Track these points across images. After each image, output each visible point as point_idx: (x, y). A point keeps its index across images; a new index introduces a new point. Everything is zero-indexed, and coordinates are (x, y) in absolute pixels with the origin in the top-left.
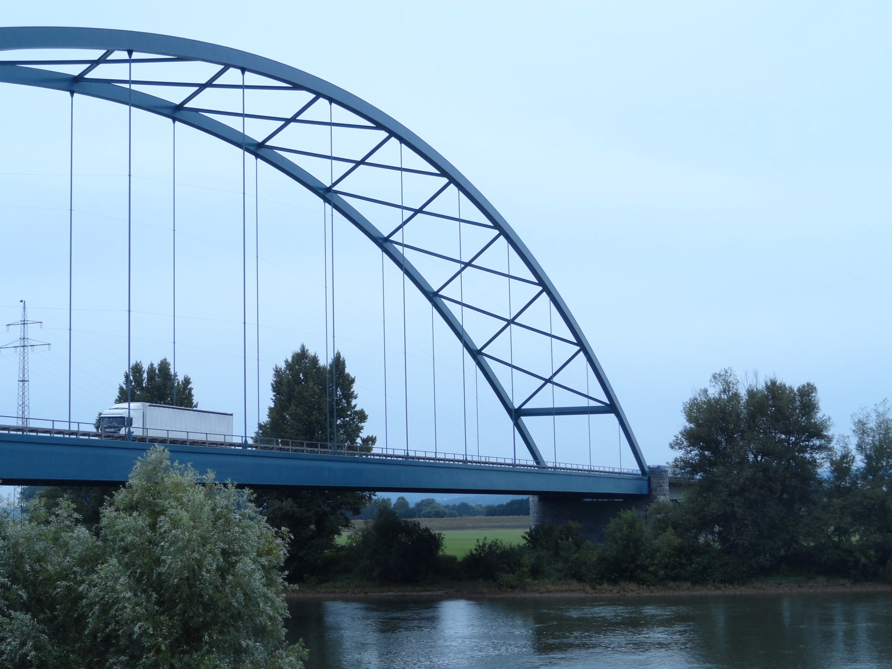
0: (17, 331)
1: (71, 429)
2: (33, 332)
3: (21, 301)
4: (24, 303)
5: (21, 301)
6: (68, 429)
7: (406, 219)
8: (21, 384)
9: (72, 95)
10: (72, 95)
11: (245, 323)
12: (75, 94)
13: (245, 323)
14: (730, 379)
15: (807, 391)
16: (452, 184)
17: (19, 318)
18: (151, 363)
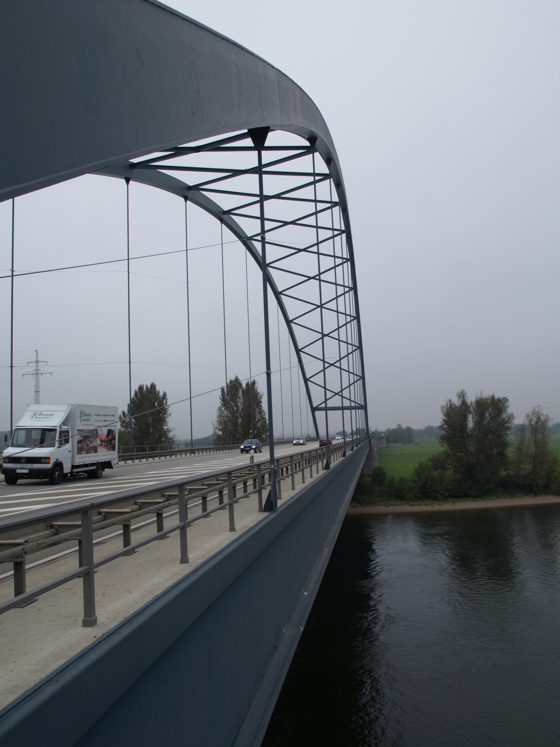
0: (33, 366)
1: (344, 406)
2: (42, 368)
3: (36, 351)
4: (37, 352)
5: (36, 351)
6: (349, 405)
7: (282, 298)
8: (36, 393)
9: (128, 183)
10: (128, 183)
11: (130, 363)
12: (131, 182)
13: (130, 363)
14: (458, 397)
15: (153, 386)
16: (260, 220)
17: (34, 359)
18: (146, 385)
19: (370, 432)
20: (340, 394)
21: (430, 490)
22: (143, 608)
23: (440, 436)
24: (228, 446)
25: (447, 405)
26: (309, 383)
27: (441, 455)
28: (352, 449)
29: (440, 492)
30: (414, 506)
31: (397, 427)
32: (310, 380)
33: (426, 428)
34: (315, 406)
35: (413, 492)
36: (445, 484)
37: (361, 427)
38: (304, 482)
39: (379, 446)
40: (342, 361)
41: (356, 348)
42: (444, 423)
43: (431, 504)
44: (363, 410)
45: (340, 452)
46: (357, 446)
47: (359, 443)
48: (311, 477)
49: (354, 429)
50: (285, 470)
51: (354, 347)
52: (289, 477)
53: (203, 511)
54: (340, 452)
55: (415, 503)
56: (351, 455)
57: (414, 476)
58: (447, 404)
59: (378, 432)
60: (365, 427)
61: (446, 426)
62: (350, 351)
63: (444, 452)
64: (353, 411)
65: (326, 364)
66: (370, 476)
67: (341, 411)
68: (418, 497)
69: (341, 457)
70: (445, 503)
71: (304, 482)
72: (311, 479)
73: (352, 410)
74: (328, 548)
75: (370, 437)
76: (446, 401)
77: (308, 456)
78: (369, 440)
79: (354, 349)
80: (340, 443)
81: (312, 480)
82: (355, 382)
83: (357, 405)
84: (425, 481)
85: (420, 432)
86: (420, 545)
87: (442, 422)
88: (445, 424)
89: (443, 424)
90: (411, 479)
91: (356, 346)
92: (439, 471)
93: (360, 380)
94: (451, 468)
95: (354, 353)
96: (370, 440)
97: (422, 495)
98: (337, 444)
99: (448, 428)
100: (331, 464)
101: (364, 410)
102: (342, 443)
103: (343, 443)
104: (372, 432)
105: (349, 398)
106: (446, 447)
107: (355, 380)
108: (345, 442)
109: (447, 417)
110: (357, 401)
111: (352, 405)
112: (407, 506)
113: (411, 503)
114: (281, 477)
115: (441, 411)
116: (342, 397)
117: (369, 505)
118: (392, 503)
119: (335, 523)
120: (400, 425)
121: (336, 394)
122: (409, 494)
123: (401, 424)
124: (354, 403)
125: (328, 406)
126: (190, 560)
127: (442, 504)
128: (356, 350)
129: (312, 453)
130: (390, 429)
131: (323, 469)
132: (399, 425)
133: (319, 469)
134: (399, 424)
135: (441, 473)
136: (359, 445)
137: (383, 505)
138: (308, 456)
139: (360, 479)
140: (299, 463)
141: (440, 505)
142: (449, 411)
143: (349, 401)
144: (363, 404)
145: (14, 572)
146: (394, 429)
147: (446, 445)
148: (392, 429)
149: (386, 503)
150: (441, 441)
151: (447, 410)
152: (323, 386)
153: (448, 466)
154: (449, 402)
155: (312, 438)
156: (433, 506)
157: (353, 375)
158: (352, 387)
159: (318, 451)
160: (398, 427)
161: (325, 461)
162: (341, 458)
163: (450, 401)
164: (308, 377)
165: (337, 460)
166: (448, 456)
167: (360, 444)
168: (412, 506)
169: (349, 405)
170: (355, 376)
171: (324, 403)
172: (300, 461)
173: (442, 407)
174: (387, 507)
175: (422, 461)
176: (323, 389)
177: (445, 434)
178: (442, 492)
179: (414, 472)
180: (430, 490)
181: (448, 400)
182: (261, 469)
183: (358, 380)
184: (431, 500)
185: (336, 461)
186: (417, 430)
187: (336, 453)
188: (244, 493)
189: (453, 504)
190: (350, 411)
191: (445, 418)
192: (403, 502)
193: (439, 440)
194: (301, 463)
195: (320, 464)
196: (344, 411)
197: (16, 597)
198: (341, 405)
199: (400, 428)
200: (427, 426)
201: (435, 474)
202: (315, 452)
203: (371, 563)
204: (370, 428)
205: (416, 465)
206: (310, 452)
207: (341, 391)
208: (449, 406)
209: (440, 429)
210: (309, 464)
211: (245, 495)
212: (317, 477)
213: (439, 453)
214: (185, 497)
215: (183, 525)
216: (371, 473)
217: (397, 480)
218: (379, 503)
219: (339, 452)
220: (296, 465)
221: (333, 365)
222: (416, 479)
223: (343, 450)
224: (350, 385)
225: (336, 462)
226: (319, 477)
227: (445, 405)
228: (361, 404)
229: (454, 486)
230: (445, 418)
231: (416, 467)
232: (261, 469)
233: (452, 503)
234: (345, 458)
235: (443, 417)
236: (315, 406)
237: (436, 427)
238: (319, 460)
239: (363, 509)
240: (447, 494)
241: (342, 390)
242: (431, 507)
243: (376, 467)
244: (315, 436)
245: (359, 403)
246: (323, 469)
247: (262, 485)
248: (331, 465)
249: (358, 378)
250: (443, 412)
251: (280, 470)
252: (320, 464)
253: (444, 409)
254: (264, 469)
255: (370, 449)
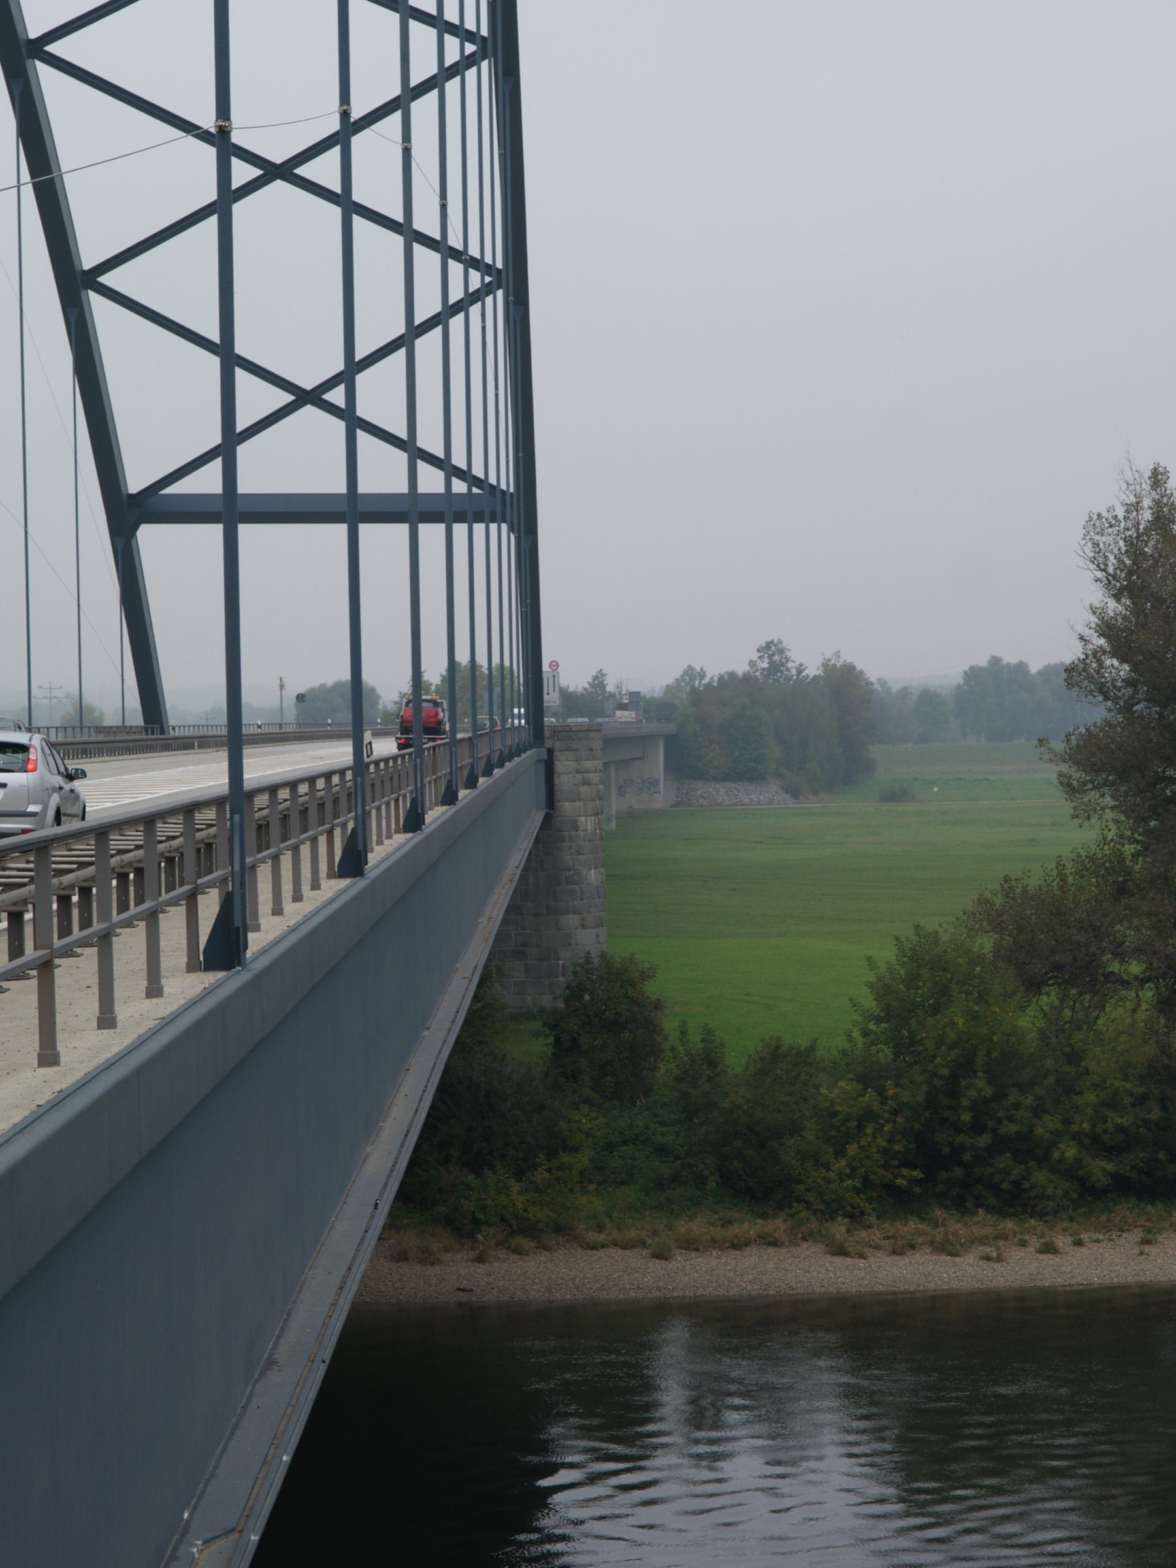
1: (363, 488)
6: (404, 488)
19: (551, 698)
20: (336, 396)
21: (985, 1140)
22: (178, 1013)
23: (1074, 742)
24: (150, 737)
25: (1136, 506)
26: (98, 305)
27: (1070, 879)
28: (414, 822)
29: (1056, 1155)
30: (862, 1256)
31: (752, 664)
32: (105, 279)
33: (973, 674)
34: (136, 481)
35: (852, 1149)
36: (1092, 1097)
37: (482, 659)
38: (48, 1056)
39: (616, 804)
40: (358, 142)
41: (470, 48)
42: (1102, 641)
43: (982, 1241)
44: (504, 526)
45: (322, 841)
46: (449, 798)
47: (466, 772)
48: (107, 1020)
49: (434, 670)
50: (29, 920)
51: (451, 42)
52: (27, 977)
53: (80, 927)
54: (322, 841)
55: (864, 1234)
56: (404, 864)
57: (866, 1033)
58: (1133, 499)
59: (612, 695)
60: (512, 658)
61: (1117, 669)
62: (423, 68)
63: (1092, 858)
64: (432, 534)
65: (237, 181)
66: (537, 1025)
67: (340, 531)
68: (890, 1187)
69: (330, 876)
70: (1084, 1236)
71: (48, 1056)
72: (277, 918)
73: (424, 529)
74: (215, 1546)
75: (547, 733)
76: (1129, 477)
77: (83, 865)
78: (544, 755)
79: (452, 55)
80: (328, 776)
81: (112, 1043)
82: (451, 310)
83: (459, 487)
84: (945, 1072)
85: (928, 699)
86: (881, 1501)
87: (1087, 633)
88: (1114, 655)
89: (1097, 654)
90: (844, 1052)
91: (470, 36)
92: (1048, 999)
93: (489, 300)
94: (1143, 982)
95: (452, 87)
96: (550, 752)
97: (917, 1174)
98: (302, 780)
99: (1128, 683)
100: (257, 928)
101: (511, 529)
102: (342, 772)
103: (349, 775)
104: (566, 695)
105: (403, 434)
106: (1111, 825)
107: (456, 294)
108: (360, 764)
109: (1132, 597)
110: (459, 460)
111: (422, 488)
112: (806, 1249)
113: (839, 1228)
114: (57, 943)
115: (1089, 550)
116: (354, 423)
117: (522, 1241)
118: (696, 1226)
119: (271, 1363)
120: (781, 651)
121: (304, 397)
122: (827, 1167)
123: (786, 643)
124: (439, 475)
125: (244, 486)
126: (262, 926)
127: (1062, 1241)
128: (469, 61)
129: (116, 842)
130: (702, 675)
131: (192, 967)
132: (771, 649)
133: (165, 962)
134: (769, 645)
135: (1067, 1013)
136: (463, 793)
137: (626, 1246)
138: (83, 865)
139: (461, 1047)
140: (85, 892)
141: (1049, 1249)
142: (1144, 554)
143: (402, 457)
144: (504, 479)
145: (9, 925)
146: (732, 675)
147: (1113, 808)
148: (721, 678)
149: (655, 1233)
150: (1078, 775)
151: (1134, 548)
152: (215, 336)
153: (1122, 961)
154: (1146, 486)
155: (109, 730)
156: (1000, 1259)
157: (435, 257)
158: (428, 346)
159: (163, 829)
160: (765, 664)
161: (209, 907)
162: (332, 887)
163: (1158, 478)
164: (89, 259)
165: (297, 897)
166: (1122, 891)
167: (471, 783)
168: (842, 1252)
169: (404, 488)
170: (455, 268)
171: (217, 464)
172: (25, 902)
173: (1097, 524)
174: (661, 1255)
175: (931, 925)
176: (212, 363)
177: (1108, 724)
178: (1070, 1151)
179: (869, 1002)
180: (985, 1140)
181: (1148, 474)
182: (197, 826)
183: (473, 298)
184: (990, 1210)
185: (289, 907)
186: (905, 692)
187: (296, 849)
188: (11, 959)
189: (1147, 1242)
190: (403, 529)
191: (1113, 607)
192: (778, 1225)
193: (1064, 768)
194: (28, 916)
195: (173, 924)
196: (364, 529)
197: (138, 908)
198: (339, 486)
199: (775, 668)
200: (983, 662)
201: (1024, 1022)
202: (136, 836)
203: (545, 1483)
204: (555, 665)
205: (887, 954)
206: (148, 821)
207: (347, 376)
208: (1147, 515)
209: (1070, 683)
210: (140, 901)
211: (170, 899)
212: (151, 1024)
213: (1060, 866)
214: (109, 861)
215: (105, 928)
216: (546, 1001)
217: (736, 1062)
218: (600, 1228)
219: (314, 840)
220: (64, 901)
221: (285, 171)
222: (885, 1053)
223: (344, 825)
224: (415, 331)
225: (294, 912)
226: (167, 1022)
227: (1120, 512)
228: (492, 480)
229: (1155, 1114)
230: (1113, 607)
231: (883, 968)
232: (197, 826)
233: (1137, 1235)
234: (362, 883)
235: (1097, 595)
236: (136, 481)
237: (1046, 672)
238: (164, 897)
239: (482, 1268)
240: (1100, 1168)
241: (353, 367)
242: (984, 1264)
243: (588, 960)
244: (136, 718)
245: (478, 471)
246: (192, 967)
247: (335, 819)
248: (251, 936)
249: (476, 280)
250: (1098, 560)
251: (55, 898)
252: (173, 924)
253: (1110, 539)
254: (204, 826)
255: (547, 821)
